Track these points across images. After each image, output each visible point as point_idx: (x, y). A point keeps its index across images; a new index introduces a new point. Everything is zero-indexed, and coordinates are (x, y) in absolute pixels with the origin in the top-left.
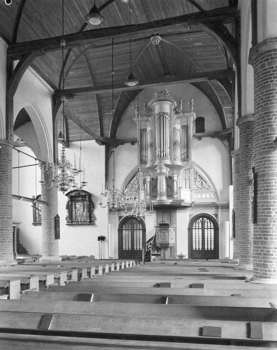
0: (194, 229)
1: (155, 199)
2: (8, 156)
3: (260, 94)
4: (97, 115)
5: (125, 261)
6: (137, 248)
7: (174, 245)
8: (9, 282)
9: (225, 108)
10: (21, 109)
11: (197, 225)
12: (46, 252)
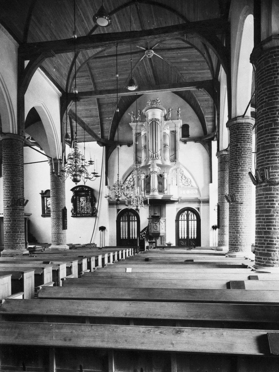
1: (149, 194)
2: (19, 151)
3: (264, 90)
5: (123, 249)
8: (23, 273)
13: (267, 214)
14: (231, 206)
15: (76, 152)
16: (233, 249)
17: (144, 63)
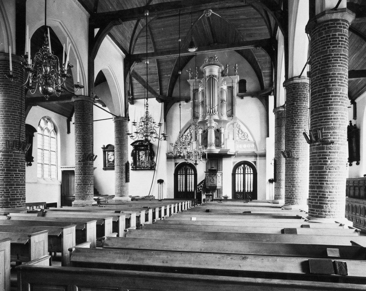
3: (318, 59)
5: (181, 201)
6: (189, 190)
8: (104, 220)
10: (100, 70)
12: (118, 193)
13: (320, 171)
14: (287, 161)
15: (147, 116)
16: (289, 202)
17: (203, 22)
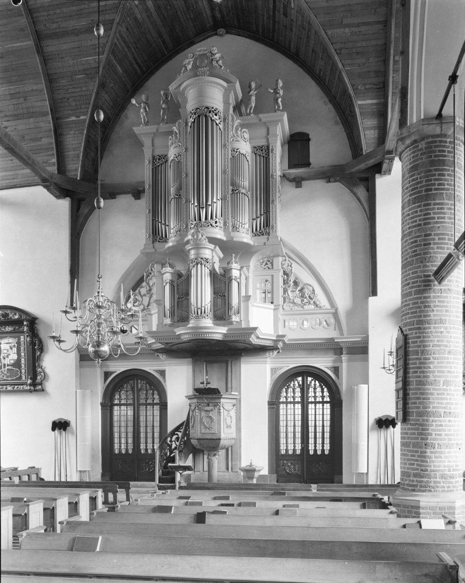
0: (283, 403)
4: (47, 123)
6: (146, 450)
7: (233, 442)
9: (363, 103)
11: (290, 394)
